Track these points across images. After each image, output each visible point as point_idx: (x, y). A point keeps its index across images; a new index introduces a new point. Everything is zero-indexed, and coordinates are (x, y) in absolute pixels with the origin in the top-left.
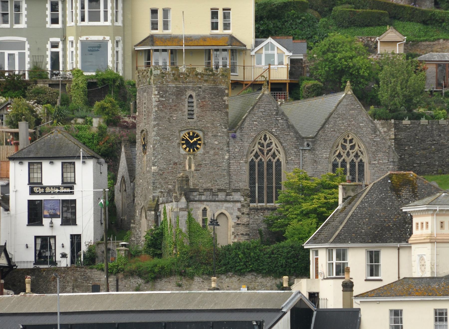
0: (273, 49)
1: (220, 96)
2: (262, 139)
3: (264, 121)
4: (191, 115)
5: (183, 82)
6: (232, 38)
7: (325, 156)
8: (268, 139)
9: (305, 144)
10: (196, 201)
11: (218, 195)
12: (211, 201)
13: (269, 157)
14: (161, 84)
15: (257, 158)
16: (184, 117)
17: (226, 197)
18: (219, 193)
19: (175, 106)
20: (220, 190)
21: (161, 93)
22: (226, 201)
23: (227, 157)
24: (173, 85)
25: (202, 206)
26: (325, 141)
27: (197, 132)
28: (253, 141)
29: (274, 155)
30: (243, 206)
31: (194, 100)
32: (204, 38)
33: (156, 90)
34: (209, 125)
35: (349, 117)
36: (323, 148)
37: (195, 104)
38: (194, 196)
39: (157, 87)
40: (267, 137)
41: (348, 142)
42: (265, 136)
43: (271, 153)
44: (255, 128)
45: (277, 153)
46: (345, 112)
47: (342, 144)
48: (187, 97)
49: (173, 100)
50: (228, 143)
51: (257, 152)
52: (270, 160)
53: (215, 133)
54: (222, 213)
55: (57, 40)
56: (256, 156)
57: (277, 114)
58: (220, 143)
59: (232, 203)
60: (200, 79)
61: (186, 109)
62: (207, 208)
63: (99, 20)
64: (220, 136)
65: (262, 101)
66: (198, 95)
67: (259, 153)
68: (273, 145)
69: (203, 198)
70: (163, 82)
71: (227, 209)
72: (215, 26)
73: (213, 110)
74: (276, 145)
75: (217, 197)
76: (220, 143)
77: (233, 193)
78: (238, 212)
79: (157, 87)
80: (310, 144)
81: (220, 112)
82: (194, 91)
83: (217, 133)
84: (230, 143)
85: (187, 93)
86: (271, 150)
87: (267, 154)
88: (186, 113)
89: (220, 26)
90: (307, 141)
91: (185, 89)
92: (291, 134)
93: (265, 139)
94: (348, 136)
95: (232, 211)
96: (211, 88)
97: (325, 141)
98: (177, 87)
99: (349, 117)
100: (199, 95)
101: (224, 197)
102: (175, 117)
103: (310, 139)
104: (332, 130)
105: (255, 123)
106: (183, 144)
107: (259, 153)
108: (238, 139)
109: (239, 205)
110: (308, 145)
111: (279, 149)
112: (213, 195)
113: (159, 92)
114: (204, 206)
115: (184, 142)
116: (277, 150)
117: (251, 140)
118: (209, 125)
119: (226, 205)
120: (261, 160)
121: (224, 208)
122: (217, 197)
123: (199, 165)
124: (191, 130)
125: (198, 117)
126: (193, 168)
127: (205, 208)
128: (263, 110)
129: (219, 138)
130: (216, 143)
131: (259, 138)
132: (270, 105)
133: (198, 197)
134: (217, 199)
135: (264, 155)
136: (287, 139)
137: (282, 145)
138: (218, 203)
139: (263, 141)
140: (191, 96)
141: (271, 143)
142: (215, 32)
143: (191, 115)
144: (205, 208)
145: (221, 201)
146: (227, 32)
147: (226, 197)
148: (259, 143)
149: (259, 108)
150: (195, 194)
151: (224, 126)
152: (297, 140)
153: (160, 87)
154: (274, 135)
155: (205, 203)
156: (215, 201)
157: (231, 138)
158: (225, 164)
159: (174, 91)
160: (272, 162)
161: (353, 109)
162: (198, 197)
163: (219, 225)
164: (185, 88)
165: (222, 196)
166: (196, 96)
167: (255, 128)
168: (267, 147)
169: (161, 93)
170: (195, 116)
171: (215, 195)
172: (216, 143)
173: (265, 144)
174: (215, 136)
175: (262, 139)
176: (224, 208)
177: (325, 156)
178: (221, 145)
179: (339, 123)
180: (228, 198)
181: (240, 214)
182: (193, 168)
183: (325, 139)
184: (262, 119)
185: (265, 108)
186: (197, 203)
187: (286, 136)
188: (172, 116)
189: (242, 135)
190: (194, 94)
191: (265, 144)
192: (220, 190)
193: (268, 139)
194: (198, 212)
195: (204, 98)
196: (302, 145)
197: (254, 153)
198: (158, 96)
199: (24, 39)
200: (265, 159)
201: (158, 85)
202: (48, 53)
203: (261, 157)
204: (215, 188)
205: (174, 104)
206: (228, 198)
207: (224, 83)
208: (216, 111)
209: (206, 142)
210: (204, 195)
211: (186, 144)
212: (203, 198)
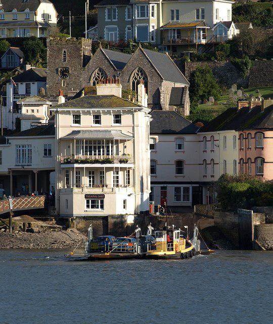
182: (65, 85)
190: (66, 50)
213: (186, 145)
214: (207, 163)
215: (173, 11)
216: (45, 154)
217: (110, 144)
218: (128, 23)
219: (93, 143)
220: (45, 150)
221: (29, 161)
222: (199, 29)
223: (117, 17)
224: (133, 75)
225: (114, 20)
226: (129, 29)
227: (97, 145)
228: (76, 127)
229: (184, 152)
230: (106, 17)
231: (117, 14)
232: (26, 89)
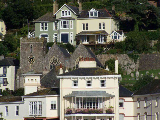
0: (116, 34)
4: (31, 51)
6: (104, 32)
9: (67, 59)
23: (42, 64)
26: (73, 58)
27: (33, 57)
32: (97, 31)
37: (33, 48)
40: (56, 57)
43: (57, 62)
51: (52, 62)
52: (77, 64)
53: (39, 57)
55: (56, 34)
56: (52, 63)
63: (66, 28)
67: (53, 62)
72: (100, 28)
82: (33, 44)
86: (57, 61)
89: (102, 28)
91: (30, 44)
93: (55, 58)
97: (73, 58)
107: (53, 62)
108: (46, 58)
110: (68, 60)
123: (34, 66)
126: (32, 67)
139: (54, 59)
140: (32, 46)
142: (100, 30)
143: (31, 51)
146: (104, 30)
158: (42, 66)
161: (82, 49)
164: (30, 43)
173: (55, 60)
182: (32, 67)
190: (32, 45)
191: (55, 60)
196: (66, 60)
197: (57, 62)
199: (47, 34)
202: (54, 38)
207: (41, 41)
213: (125, 104)
214: (125, 116)
215: (84, 25)
216: (52, 108)
217: (99, 101)
218: (55, 32)
219: (86, 100)
220: (52, 105)
221: (39, 112)
222: (102, 35)
223: (47, 28)
224: (76, 60)
225: (46, 30)
226: (56, 35)
227: (89, 101)
228: (76, 89)
229: (124, 108)
230: (41, 28)
231: (47, 26)
232: (4, 70)
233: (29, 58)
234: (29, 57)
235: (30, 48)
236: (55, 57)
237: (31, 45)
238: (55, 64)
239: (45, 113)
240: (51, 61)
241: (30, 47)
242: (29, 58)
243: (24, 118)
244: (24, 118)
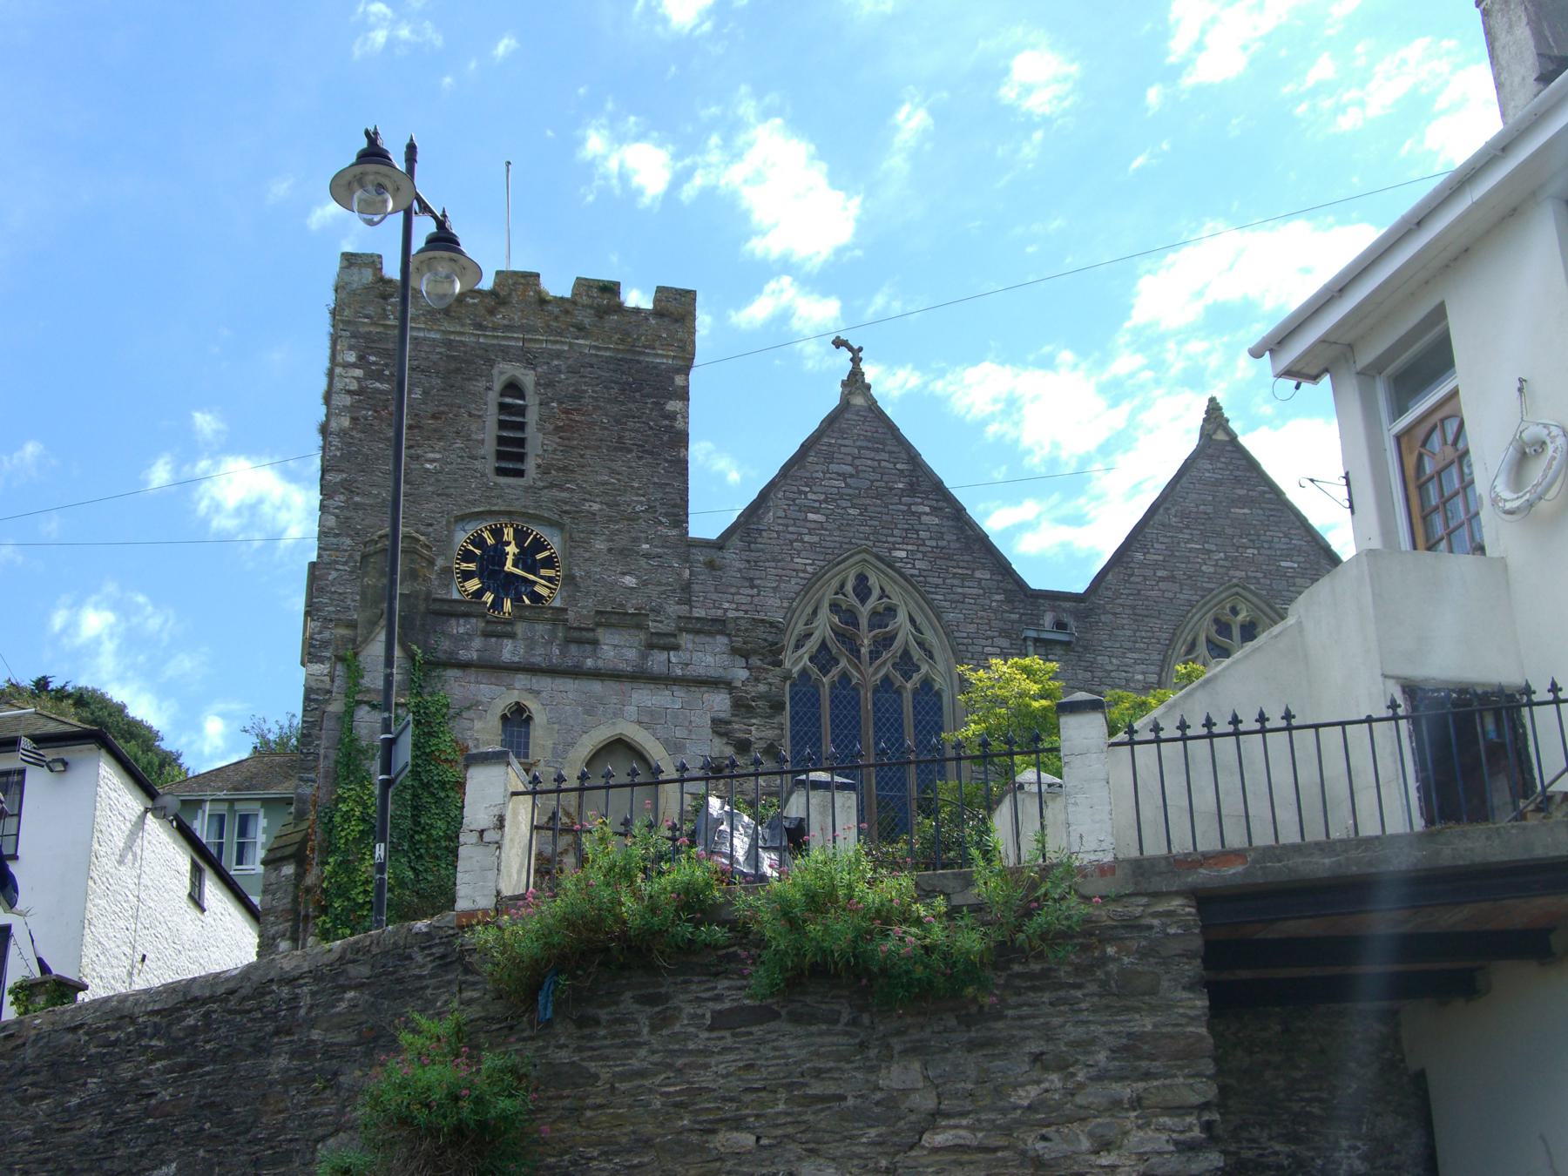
1: (649, 396)
2: (849, 587)
3: (851, 511)
4: (511, 455)
5: (479, 326)
7: (1140, 677)
8: (876, 593)
9: (1048, 619)
10: (465, 666)
11: (595, 643)
12: (553, 672)
13: (886, 666)
14: (374, 324)
15: (825, 670)
16: (478, 464)
17: (644, 657)
18: (603, 635)
19: (434, 417)
20: (616, 618)
21: (373, 359)
22: (640, 676)
24: (433, 335)
25: (500, 697)
28: (806, 589)
29: (906, 664)
30: (741, 706)
31: (532, 401)
33: (351, 348)
34: (596, 507)
35: (1229, 531)
36: (1128, 645)
37: (532, 417)
38: (458, 639)
39: (353, 336)
40: (873, 581)
41: (1236, 632)
42: (862, 579)
44: (816, 539)
45: (916, 653)
46: (1210, 509)
47: (1209, 641)
48: (498, 386)
49: (425, 393)
50: (687, 587)
51: (824, 645)
54: (620, 746)
56: (824, 658)
57: (912, 489)
58: (645, 583)
59: (680, 692)
60: (556, 318)
61: (488, 433)
62: (532, 705)
64: (647, 556)
65: (842, 431)
66: (545, 383)
67: (835, 647)
68: (902, 617)
69: (509, 651)
70: (386, 317)
71: (649, 720)
73: (616, 449)
74: (912, 620)
75: (594, 655)
76: (645, 583)
77: (685, 640)
78: (717, 740)
79: (353, 336)
80: (1072, 623)
81: (649, 459)
83: (636, 540)
84: (696, 587)
85: (495, 371)
86: (888, 640)
87: (875, 655)
88: (490, 447)
90: (1053, 609)
92: (978, 574)
93: (863, 591)
94: (1234, 611)
95: (680, 733)
96: (608, 360)
98: (449, 344)
99: (1229, 531)
100: (550, 384)
101: (632, 654)
102: (432, 461)
103: (1067, 605)
104: (1159, 573)
105: (811, 516)
106: (467, 576)
109: (720, 702)
110: (1060, 626)
111: (929, 636)
112: (568, 641)
113: (361, 358)
114: (513, 697)
115: (472, 566)
116: (921, 644)
117: (793, 586)
118: (596, 507)
119: (645, 697)
120: (845, 677)
121: (631, 710)
122: (594, 655)
124: (503, 520)
125: (544, 470)
127: (519, 709)
128: (849, 469)
129: (643, 562)
130: (630, 581)
131: (835, 583)
132: (877, 450)
133: (477, 643)
134: (589, 663)
135: (858, 658)
136: (964, 595)
137: (939, 618)
138: (597, 687)
140: (513, 388)
141: (891, 611)
143: (511, 455)
144: (519, 709)
145: (615, 676)
147: (644, 657)
148: (835, 607)
149: (829, 458)
150: (459, 627)
151: (666, 515)
152: (1008, 601)
153: (368, 337)
154: (902, 575)
155: (521, 680)
156: (576, 673)
157: (699, 568)
159: (435, 357)
160: (899, 692)
162: (477, 643)
163: (372, 137)
165: (616, 649)
166: (537, 384)
167: (816, 539)
168: (872, 627)
169: (373, 359)
170: (530, 465)
171: (580, 642)
172: (630, 581)
173: (864, 612)
174: (624, 553)
175: (849, 587)
176: (631, 710)
177: (1140, 677)
178: (653, 591)
179: (1191, 550)
180: (657, 661)
181: (729, 751)
183: (1134, 607)
184: (844, 503)
185: (857, 462)
186: (472, 674)
187: (956, 582)
188: (418, 457)
189: (754, 564)
190: (528, 379)
191: (864, 612)
192: (616, 618)
193: (876, 593)
194: (478, 725)
195: (577, 396)
196: (1035, 622)
197: (812, 645)
198: (359, 373)
200: (869, 675)
201: (363, 330)
203: (843, 663)
204: (582, 611)
205: (431, 408)
206: (657, 661)
208: (630, 451)
209: (577, 572)
210: (512, 636)
211: (479, 574)
212: (509, 651)
229: (374, 173)
233: (478, 541)
234: (471, 529)
235: (492, 416)
236: (862, 579)
237: (507, 370)
238: (869, 675)
239: (1065, 482)
240: (800, 628)
241: (493, 398)
242: (478, 541)
243: (1256, 353)
244: (1256, 353)
